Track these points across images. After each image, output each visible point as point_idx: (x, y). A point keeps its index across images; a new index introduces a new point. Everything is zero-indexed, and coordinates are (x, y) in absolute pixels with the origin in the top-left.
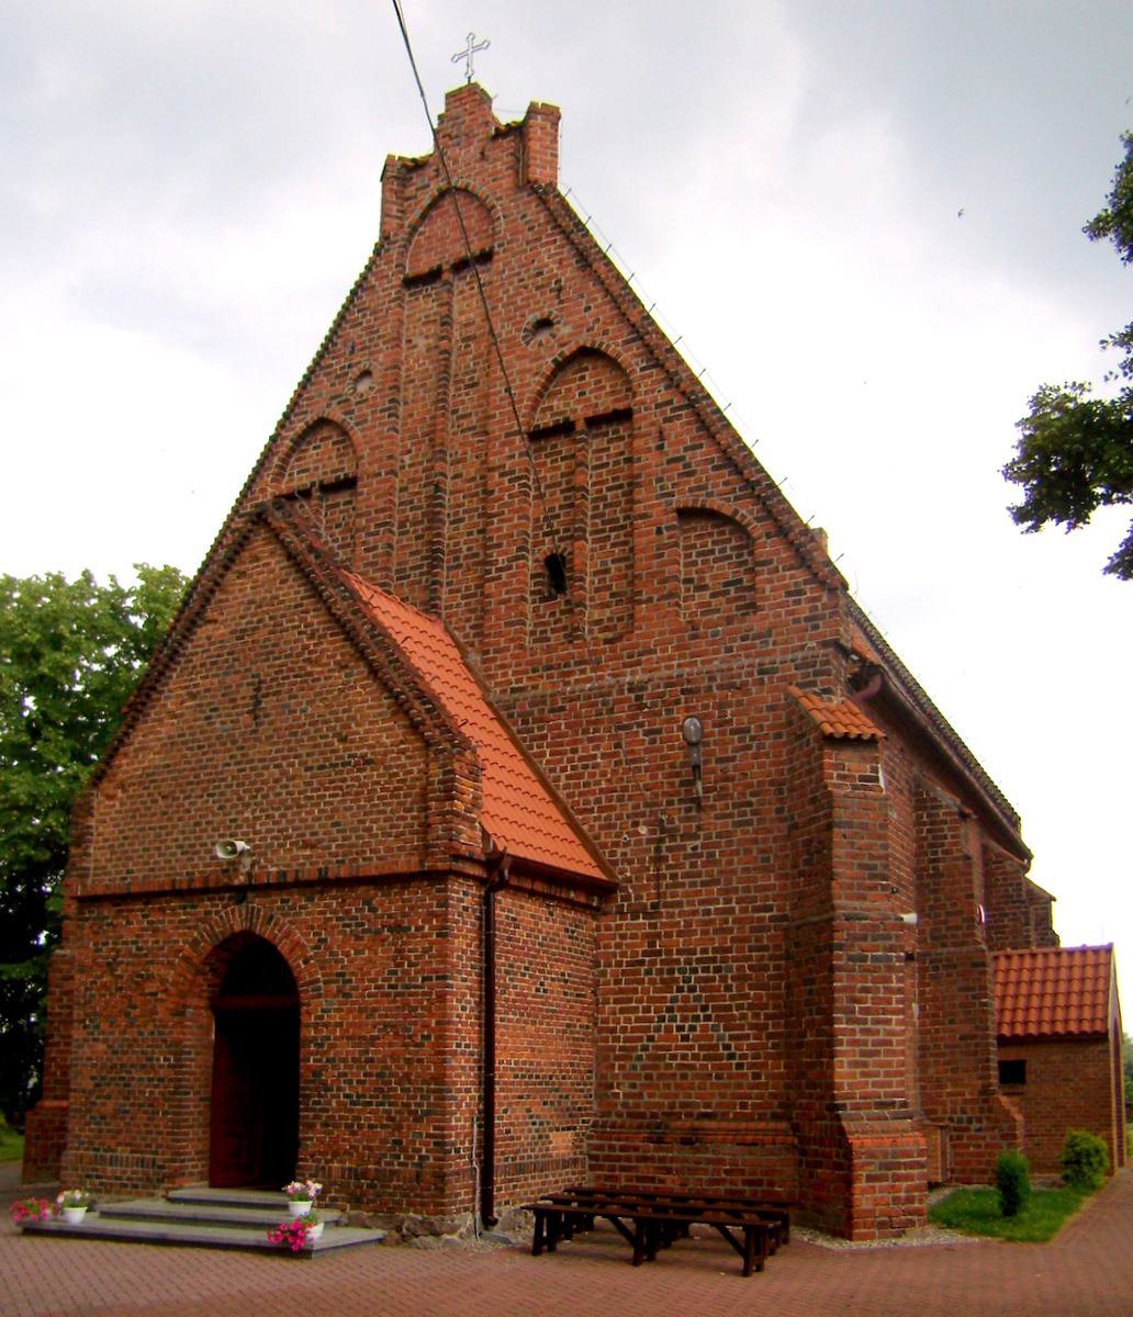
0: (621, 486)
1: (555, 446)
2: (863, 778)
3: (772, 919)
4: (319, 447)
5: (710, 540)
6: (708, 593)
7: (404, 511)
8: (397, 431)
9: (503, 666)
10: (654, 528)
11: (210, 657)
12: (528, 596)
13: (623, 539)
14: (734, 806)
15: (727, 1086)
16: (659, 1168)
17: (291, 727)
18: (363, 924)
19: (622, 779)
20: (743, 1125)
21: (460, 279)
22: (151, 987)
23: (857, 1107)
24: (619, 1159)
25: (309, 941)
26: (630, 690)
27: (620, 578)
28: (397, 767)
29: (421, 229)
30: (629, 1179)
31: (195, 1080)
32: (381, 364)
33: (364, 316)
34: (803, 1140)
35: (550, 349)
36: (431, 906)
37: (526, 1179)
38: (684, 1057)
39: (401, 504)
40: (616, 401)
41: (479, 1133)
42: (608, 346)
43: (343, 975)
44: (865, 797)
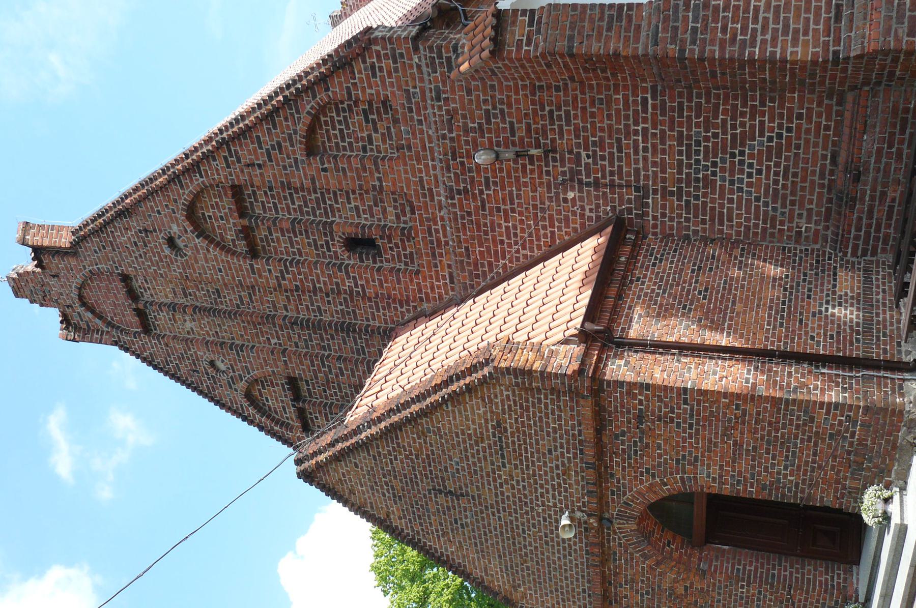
0: (291, 194)
1: (262, 240)
2: (531, 24)
3: (654, 98)
4: (267, 399)
5: (332, 132)
6: (374, 135)
7: (312, 346)
8: (253, 347)
9: (432, 288)
10: (322, 173)
11: (415, 518)
12: (377, 266)
13: (331, 195)
14: (552, 124)
15: (807, 141)
16: (880, 201)
17: (469, 473)
18: (635, 442)
19: (526, 209)
20: (846, 130)
21: (143, 296)
22: (680, 590)
23: (837, 41)
24: (868, 234)
25: (647, 481)
26: (453, 198)
27: (362, 199)
28: (503, 405)
29: (109, 319)
30: (888, 226)
31: (762, 567)
32: (205, 353)
33: (171, 361)
34: (866, 82)
35: (190, 241)
36: (622, 393)
37: (878, 323)
38: (777, 174)
39: (307, 347)
40: (226, 194)
41: (830, 368)
42: (185, 199)
43: (678, 461)
44: (547, 24)
